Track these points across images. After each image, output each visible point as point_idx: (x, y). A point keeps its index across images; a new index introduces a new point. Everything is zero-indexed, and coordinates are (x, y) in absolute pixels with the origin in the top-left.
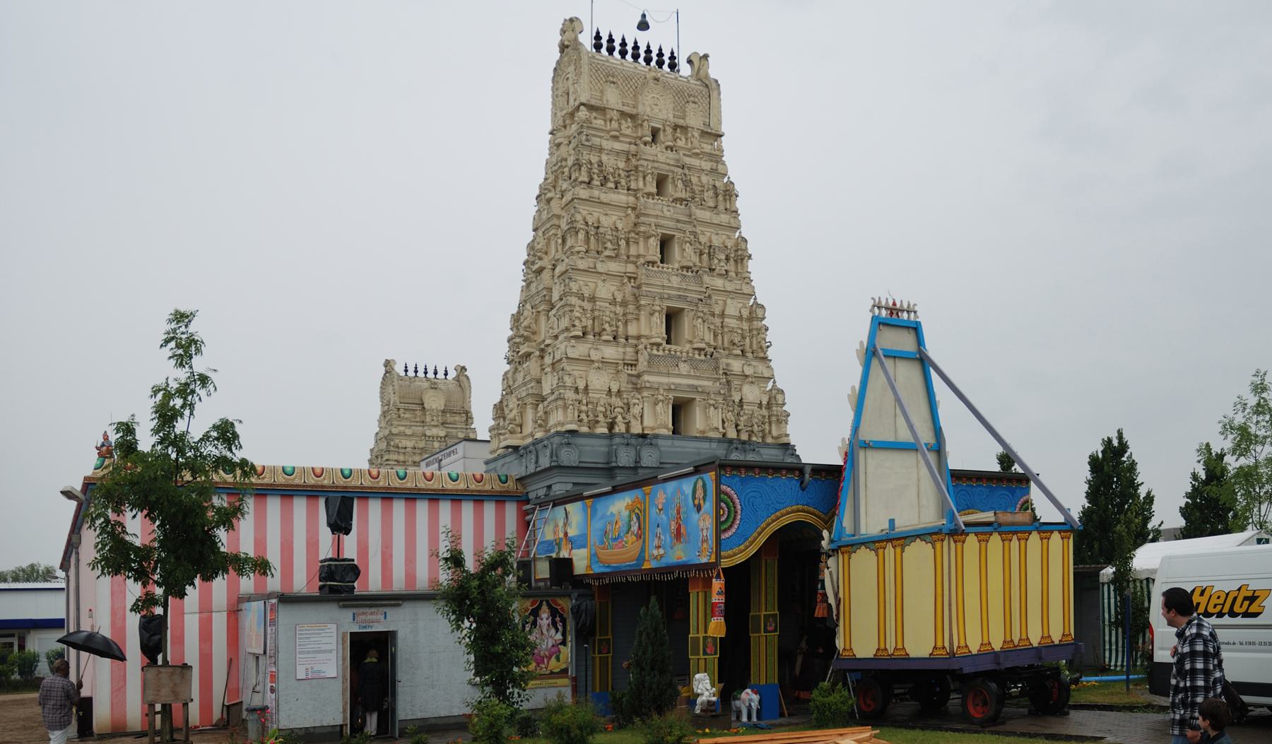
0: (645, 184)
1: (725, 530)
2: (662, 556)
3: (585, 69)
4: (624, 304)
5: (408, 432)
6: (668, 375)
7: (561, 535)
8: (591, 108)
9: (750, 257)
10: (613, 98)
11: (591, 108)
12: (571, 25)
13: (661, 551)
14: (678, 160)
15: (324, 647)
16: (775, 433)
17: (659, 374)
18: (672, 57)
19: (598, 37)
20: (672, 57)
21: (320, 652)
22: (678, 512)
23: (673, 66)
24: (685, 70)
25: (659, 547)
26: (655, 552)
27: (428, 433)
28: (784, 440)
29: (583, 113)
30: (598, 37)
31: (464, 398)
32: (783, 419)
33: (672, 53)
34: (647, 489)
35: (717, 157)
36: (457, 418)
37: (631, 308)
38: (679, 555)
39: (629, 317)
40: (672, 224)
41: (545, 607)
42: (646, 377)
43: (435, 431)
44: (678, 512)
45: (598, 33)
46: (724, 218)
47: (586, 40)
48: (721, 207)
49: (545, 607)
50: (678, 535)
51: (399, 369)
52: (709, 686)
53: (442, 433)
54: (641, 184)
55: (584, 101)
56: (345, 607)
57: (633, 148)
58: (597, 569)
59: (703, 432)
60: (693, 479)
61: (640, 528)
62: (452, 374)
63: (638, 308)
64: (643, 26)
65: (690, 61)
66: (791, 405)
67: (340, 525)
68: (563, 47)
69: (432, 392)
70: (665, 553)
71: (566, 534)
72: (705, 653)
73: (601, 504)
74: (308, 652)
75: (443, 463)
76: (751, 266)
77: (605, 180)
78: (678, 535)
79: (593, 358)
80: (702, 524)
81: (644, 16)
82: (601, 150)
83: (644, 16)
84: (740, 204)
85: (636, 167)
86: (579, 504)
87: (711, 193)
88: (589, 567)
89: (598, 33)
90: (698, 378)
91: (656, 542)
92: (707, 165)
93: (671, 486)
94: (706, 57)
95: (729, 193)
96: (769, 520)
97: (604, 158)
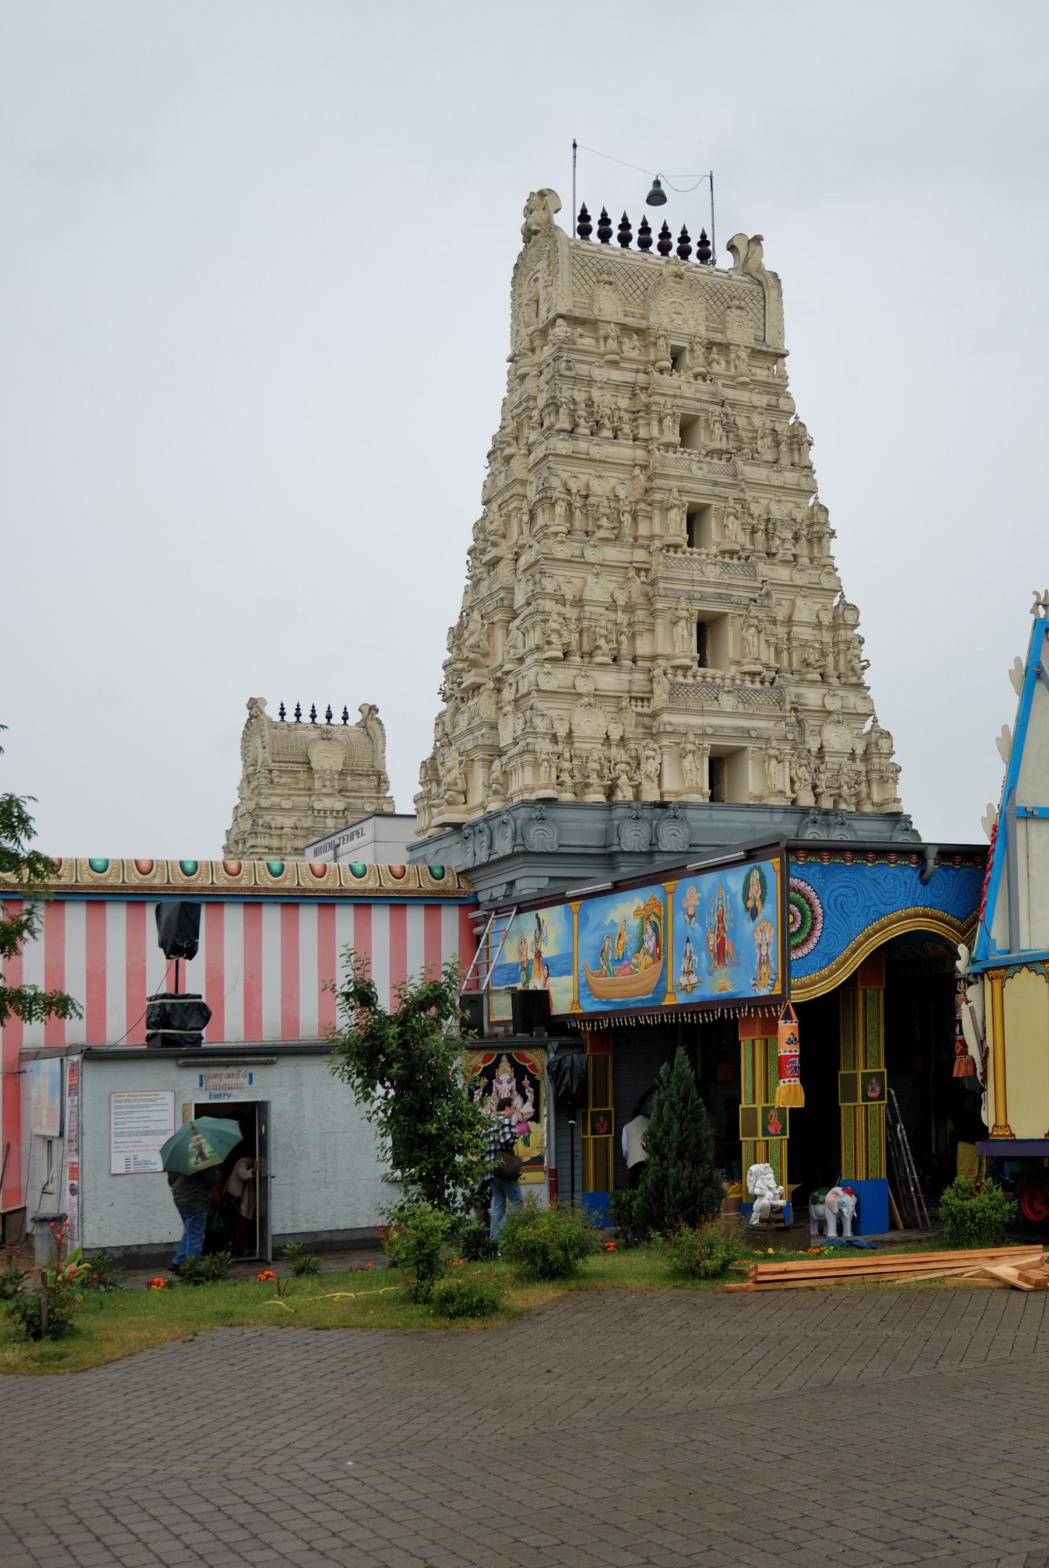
0: (661, 431)
1: (798, 946)
2: (694, 986)
3: (564, 264)
4: (630, 608)
5: (286, 804)
6: (702, 712)
7: (531, 956)
8: (573, 321)
9: (832, 534)
10: (608, 306)
11: (573, 321)
12: (542, 201)
13: (693, 979)
14: (714, 394)
15: (154, 1126)
16: (876, 797)
17: (688, 711)
18: (704, 242)
19: (584, 217)
20: (704, 242)
21: (146, 1133)
22: (721, 919)
23: (704, 256)
24: (724, 260)
25: (689, 973)
26: (684, 981)
27: (317, 805)
28: (893, 808)
29: (562, 329)
30: (584, 217)
31: (374, 752)
32: (890, 775)
33: (703, 236)
34: (669, 885)
35: (777, 388)
36: (364, 783)
37: (641, 614)
38: (722, 984)
39: (638, 627)
40: (705, 488)
41: (505, 1064)
42: (666, 717)
43: (328, 803)
44: (721, 919)
45: (584, 211)
46: (790, 477)
47: (566, 222)
48: (785, 461)
49: (505, 1064)
50: (721, 954)
51: (272, 712)
52: (772, 1183)
53: (340, 805)
54: (655, 431)
55: (562, 310)
56: (186, 1066)
57: (642, 378)
58: (589, 1006)
59: (761, 798)
60: (745, 869)
61: (657, 943)
62: (355, 718)
63: (653, 614)
64: (656, 198)
65: (731, 248)
66: (903, 754)
67: (180, 942)
68: (529, 234)
69: (322, 745)
70: (698, 981)
71: (538, 954)
72: (766, 1132)
73: (596, 910)
74: (130, 1134)
75: (342, 849)
76: (835, 547)
77: (597, 427)
78: (721, 954)
79: (830, 707)
80: (759, 938)
81: (657, 183)
82: (591, 382)
83: (657, 183)
84: (814, 456)
85: (648, 406)
86: (559, 909)
87: (768, 441)
88: (577, 1003)
89: (584, 211)
90: (751, 716)
91: (684, 965)
92: (761, 400)
93: (708, 880)
94: (758, 239)
95: (798, 440)
96: (869, 930)
97: (596, 394)
